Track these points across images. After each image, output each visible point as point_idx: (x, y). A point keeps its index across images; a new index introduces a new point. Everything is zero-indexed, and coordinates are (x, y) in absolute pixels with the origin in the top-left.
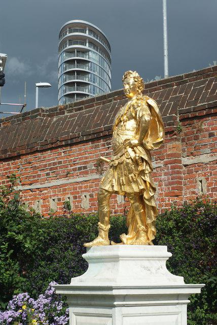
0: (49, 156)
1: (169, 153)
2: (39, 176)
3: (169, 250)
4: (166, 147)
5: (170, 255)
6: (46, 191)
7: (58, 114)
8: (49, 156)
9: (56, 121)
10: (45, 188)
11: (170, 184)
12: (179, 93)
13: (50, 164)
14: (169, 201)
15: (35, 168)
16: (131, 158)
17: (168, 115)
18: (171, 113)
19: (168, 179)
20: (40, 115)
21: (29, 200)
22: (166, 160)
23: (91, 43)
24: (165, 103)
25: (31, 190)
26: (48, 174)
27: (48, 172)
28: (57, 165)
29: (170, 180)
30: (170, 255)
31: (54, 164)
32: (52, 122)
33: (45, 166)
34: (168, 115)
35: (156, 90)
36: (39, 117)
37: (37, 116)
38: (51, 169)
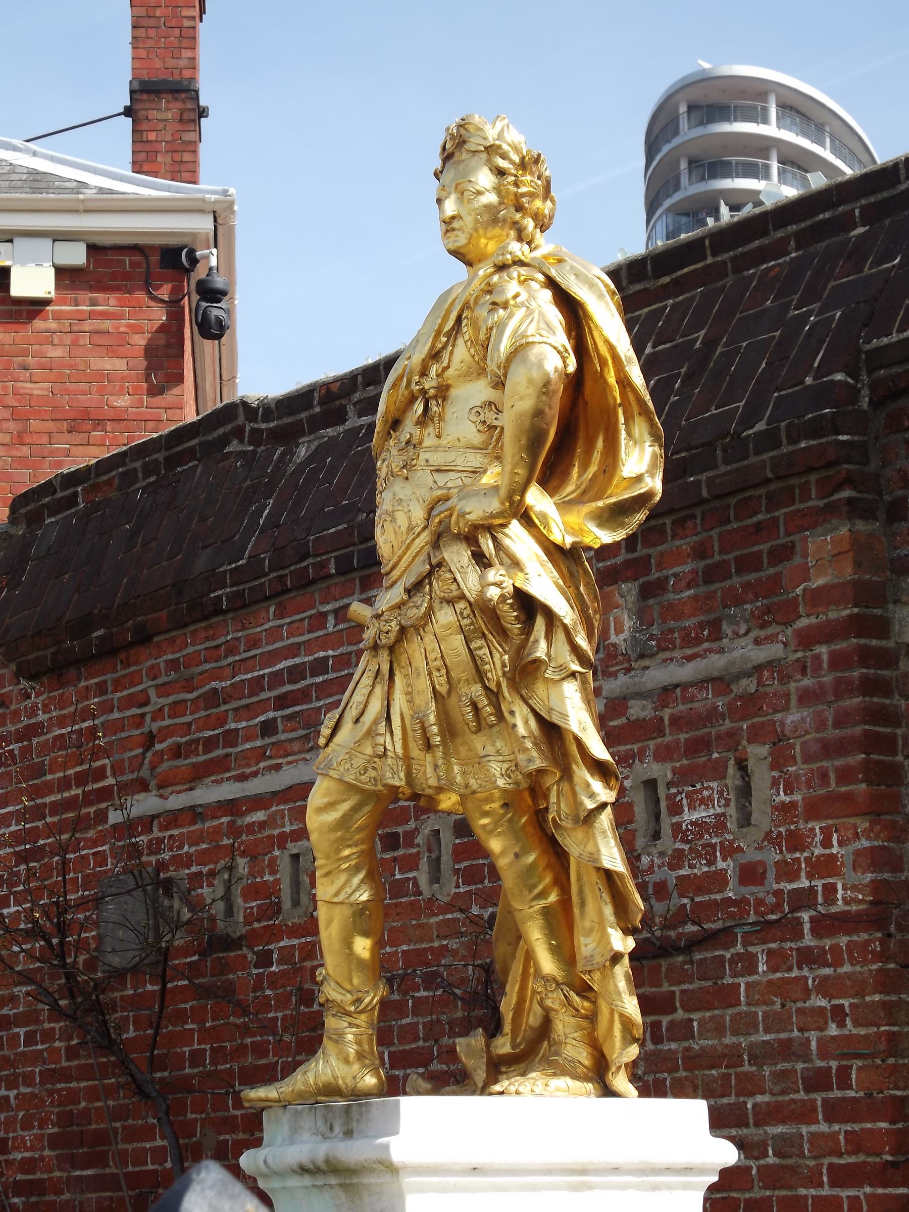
0: (274, 634)
1: (820, 582)
2: (231, 738)
3: (719, 1123)
4: (805, 555)
5: (727, 1154)
6: (260, 816)
7: (316, 424)
8: (274, 634)
9: (309, 459)
10: (258, 802)
11: (829, 749)
12: (877, 263)
13: (276, 679)
14: (827, 843)
15: (213, 698)
16: (463, 597)
17: (809, 380)
18: (827, 368)
19: (821, 724)
20: (238, 433)
21: (188, 861)
22: (803, 622)
23: (793, 164)
24: (804, 318)
25: (195, 813)
26: (268, 728)
27: (271, 714)
28: (309, 681)
29: (832, 733)
30: (727, 1154)
31: (296, 674)
32: (292, 468)
33: (257, 685)
34: (809, 380)
35: (763, 255)
36: (234, 446)
37: (225, 440)
38: (281, 702)
